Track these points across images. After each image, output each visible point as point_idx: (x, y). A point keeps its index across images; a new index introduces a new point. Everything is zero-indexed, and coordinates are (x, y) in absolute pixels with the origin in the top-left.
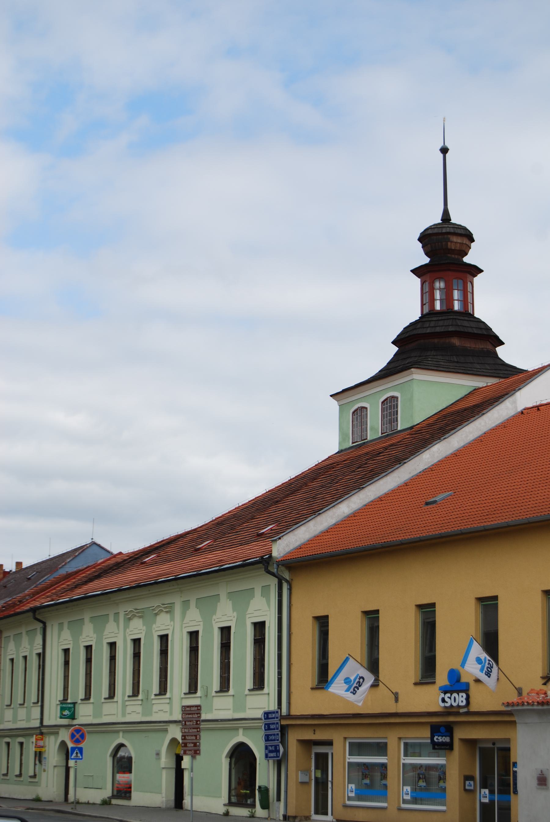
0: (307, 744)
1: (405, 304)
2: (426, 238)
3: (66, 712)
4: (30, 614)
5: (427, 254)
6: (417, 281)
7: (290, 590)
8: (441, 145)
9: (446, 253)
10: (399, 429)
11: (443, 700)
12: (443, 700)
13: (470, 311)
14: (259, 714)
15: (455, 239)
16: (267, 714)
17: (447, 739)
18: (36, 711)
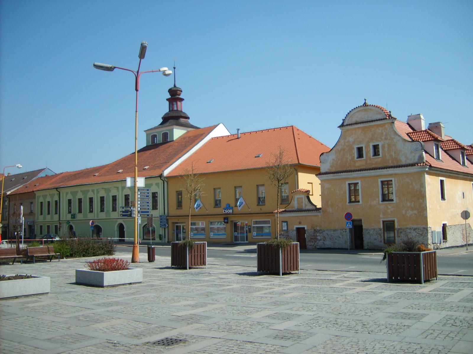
0: (174, 223)
1: (165, 109)
2: (170, 91)
3: (73, 217)
4: (56, 190)
5: (170, 95)
6: (168, 103)
7: (167, 184)
8: (173, 66)
9: (175, 96)
10: (169, 141)
11: (224, 211)
12: (224, 211)
13: (179, 109)
14: (158, 216)
15: (178, 92)
16: (161, 216)
17: (227, 221)
18: (57, 216)
